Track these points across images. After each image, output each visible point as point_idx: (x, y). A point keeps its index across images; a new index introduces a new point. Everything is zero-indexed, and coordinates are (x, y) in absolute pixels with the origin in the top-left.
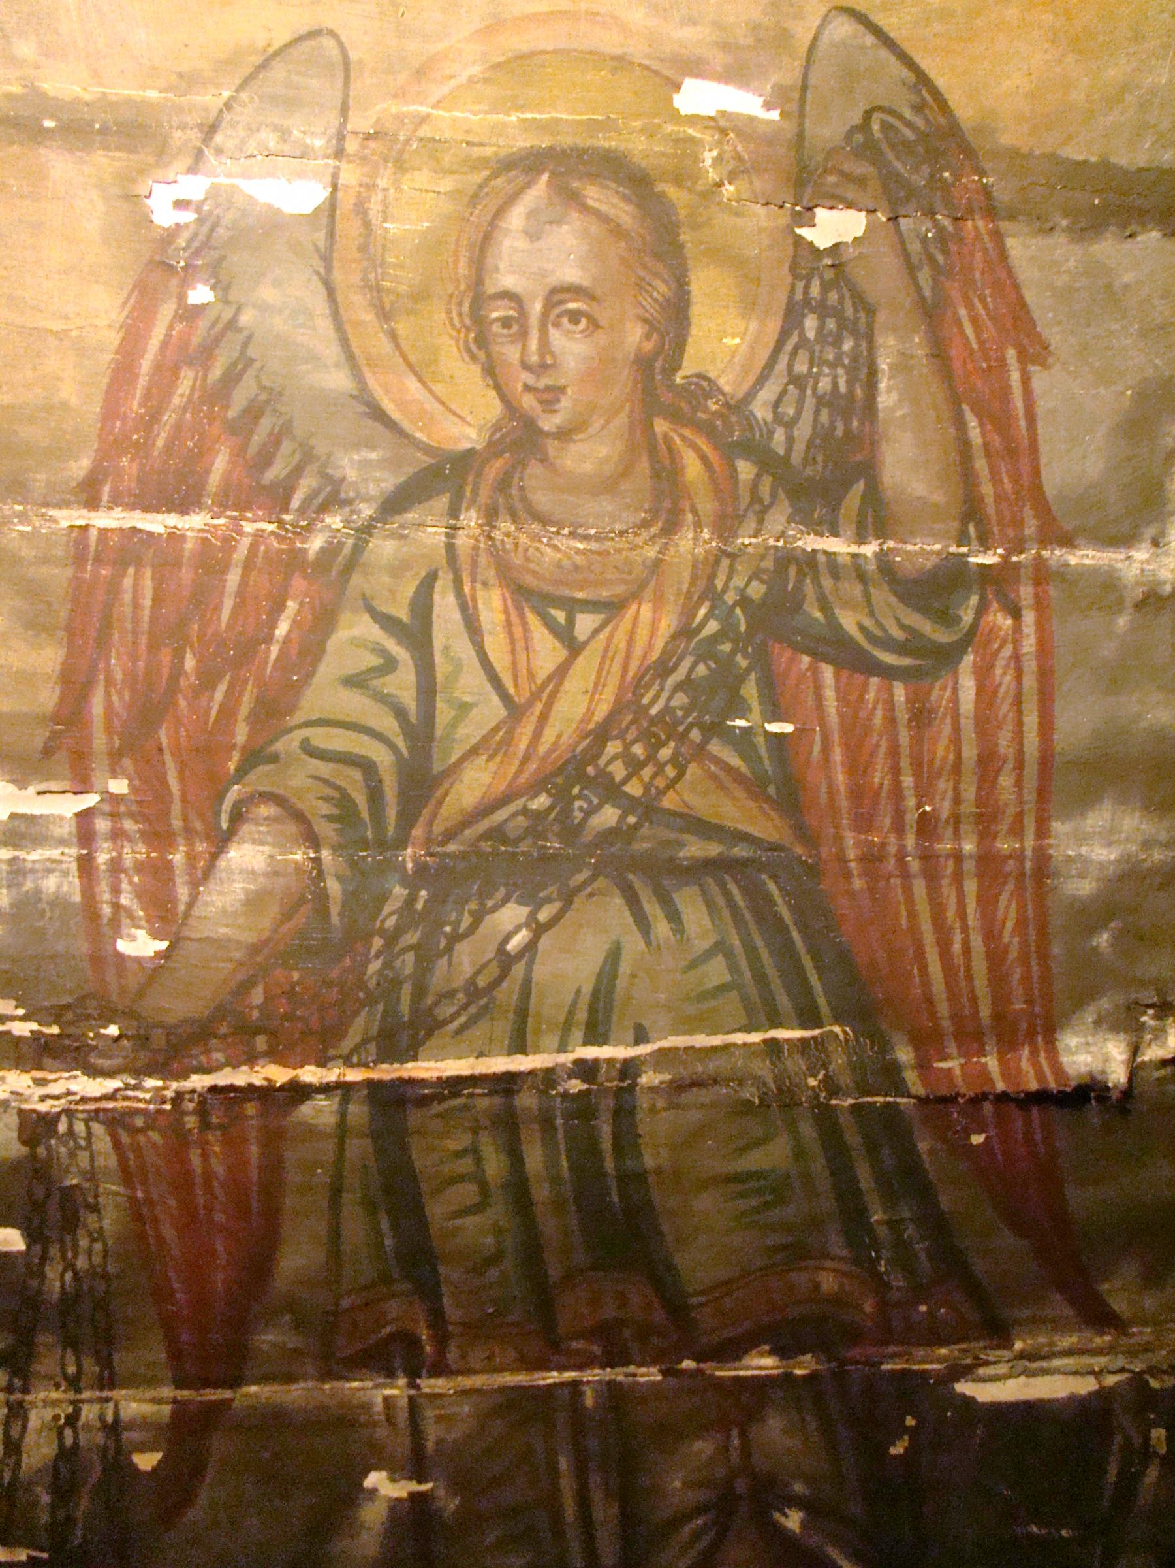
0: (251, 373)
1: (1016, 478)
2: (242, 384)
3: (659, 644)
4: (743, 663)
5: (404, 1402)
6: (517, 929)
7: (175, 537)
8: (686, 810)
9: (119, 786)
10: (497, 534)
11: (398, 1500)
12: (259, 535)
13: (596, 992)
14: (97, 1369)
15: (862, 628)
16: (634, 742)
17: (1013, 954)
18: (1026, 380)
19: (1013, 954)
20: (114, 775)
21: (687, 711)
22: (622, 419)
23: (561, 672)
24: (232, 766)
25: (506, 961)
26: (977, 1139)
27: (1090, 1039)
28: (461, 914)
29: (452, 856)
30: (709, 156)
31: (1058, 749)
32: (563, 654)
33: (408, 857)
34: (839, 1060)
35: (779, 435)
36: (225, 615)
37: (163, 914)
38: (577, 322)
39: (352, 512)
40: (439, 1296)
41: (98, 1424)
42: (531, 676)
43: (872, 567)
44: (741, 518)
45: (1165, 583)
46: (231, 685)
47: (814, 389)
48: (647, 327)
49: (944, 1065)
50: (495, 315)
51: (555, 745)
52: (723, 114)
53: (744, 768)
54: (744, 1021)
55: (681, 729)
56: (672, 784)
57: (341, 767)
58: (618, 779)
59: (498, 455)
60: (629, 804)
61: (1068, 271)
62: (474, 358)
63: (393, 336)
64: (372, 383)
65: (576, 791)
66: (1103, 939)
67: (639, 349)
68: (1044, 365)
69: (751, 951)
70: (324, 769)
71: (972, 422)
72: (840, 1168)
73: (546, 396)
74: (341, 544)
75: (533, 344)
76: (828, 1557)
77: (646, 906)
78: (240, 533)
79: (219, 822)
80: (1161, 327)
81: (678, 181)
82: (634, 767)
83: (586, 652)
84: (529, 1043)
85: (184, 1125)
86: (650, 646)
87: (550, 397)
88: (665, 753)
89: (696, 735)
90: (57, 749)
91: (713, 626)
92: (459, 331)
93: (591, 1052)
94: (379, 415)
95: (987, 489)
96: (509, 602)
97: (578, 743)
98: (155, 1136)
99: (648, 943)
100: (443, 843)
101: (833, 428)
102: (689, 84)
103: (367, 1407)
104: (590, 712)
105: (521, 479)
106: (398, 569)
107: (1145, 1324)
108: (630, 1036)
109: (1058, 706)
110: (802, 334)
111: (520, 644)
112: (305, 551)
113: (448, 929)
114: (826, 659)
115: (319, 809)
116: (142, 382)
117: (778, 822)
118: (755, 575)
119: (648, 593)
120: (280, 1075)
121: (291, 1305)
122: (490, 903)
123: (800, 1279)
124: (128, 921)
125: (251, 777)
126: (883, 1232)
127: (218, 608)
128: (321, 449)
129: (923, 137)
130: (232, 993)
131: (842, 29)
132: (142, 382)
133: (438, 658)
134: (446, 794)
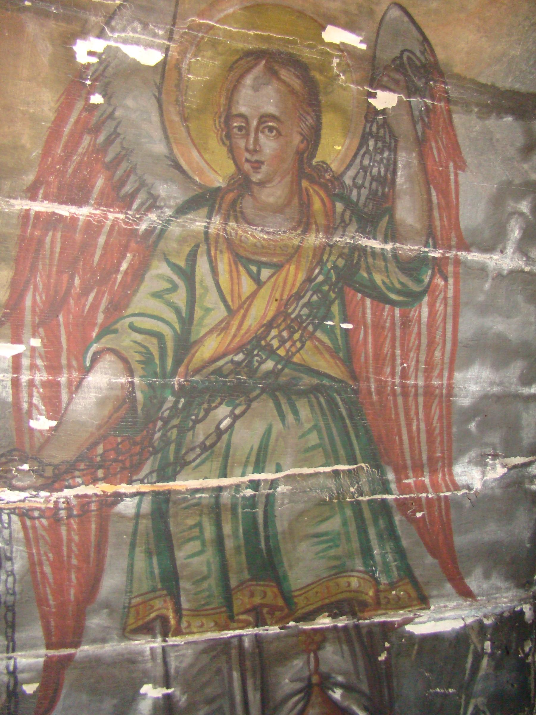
0: (118, 140)
1: (449, 220)
2: (113, 145)
3: (298, 284)
4: (333, 296)
5: (160, 650)
6: (225, 418)
7: (74, 219)
8: (303, 363)
9: (36, 342)
10: (228, 229)
11: (158, 698)
12: (115, 222)
13: (260, 449)
14: (6, 643)
15: (384, 283)
16: (283, 330)
17: (437, 431)
18: (456, 175)
19: (437, 431)
20: (34, 336)
21: (308, 316)
22: (288, 179)
23: (253, 295)
24: (94, 334)
25: (219, 433)
26: (419, 515)
27: (466, 469)
28: (200, 410)
29: (197, 382)
30: (335, 61)
31: (459, 340)
32: (255, 287)
33: (177, 381)
34: (364, 480)
35: (355, 192)
36: (97, 258)
37: (54, 409)
38: (272, 132)
39: (162, 213)
40: (179, 596)
41: (5, 671)
42: (240, 296)
43: (389, 255)
44: (336, 229)
45: (504, 270)
46: (97, 293)
47: (371, 172)
48: (302, 138)
49: (406, 481)
50: (235, 124)
51: (248, 330)
52: (342, 43)
53: (330, 345)
54: (324, 461)
55: (304, 325)
56: (298, 351)
57: (148, 337)
58: (275, 347)
59: (232, 191)
60: (279, 360)
61: (476, 131)
62: (224, 144)
63: (188, 129)
64: (175, 151)
65: (255, 352)
66: (472, 426)
67: (298, 146)
68: (464, 171)
69: (328, 428)
70: (139, 337)
71: (434, 193)
72: (362, 530)
73: (255, 165)
74: (155, 228)
75: (251, 141)
76: (351, 709)
77: (284, 408)
78: (107, 219)
79: (85, 362)
80: (509, 159)
81: (321, 72)
82: (283, 342)
83: (265, 287)
84: (228, 472)
85: (59, 515)
86: (293, 285)
87: (257, 165)
88: (296, 336)
89: (310, 328)
90: (4, 321)
91: (321, 278)
92: (218, 130)
93: (256, 476)
94: (177, 166)
95: (438, 223)
96: (232, 261)
97: (258, 330)
98: (44, 521)
99: (284, 424)
100: (193, 376)
101: (377, 190)
102: (329, 28)
103: (141, 653)
104: (265, 315)
105: (241, 203)
106: (182, 240)
107: (483, 595)
108: (274, 468)
109: (461, 320)
110: (368, 147)
111: (236, 281)
112: (137, 230)
113: (193, 417)
114: (369, 296)
115: (135, 358)
116: (64, 139)
117: (343, 369)
118: (341, 255)
119: (295, 259)
120: (109, 488)
121: (107, 605)
122: (213, 405)
123: (343, 581)
124: (36, 411)
125: (103, 340)
126: (378, 558)
127: (93, 255)
128: (149, 179)
129: (424, 66)
130: (88, 449)
131: (395, 13)
132: (64, 139)
133: (197, 285)
134: (196, 352)
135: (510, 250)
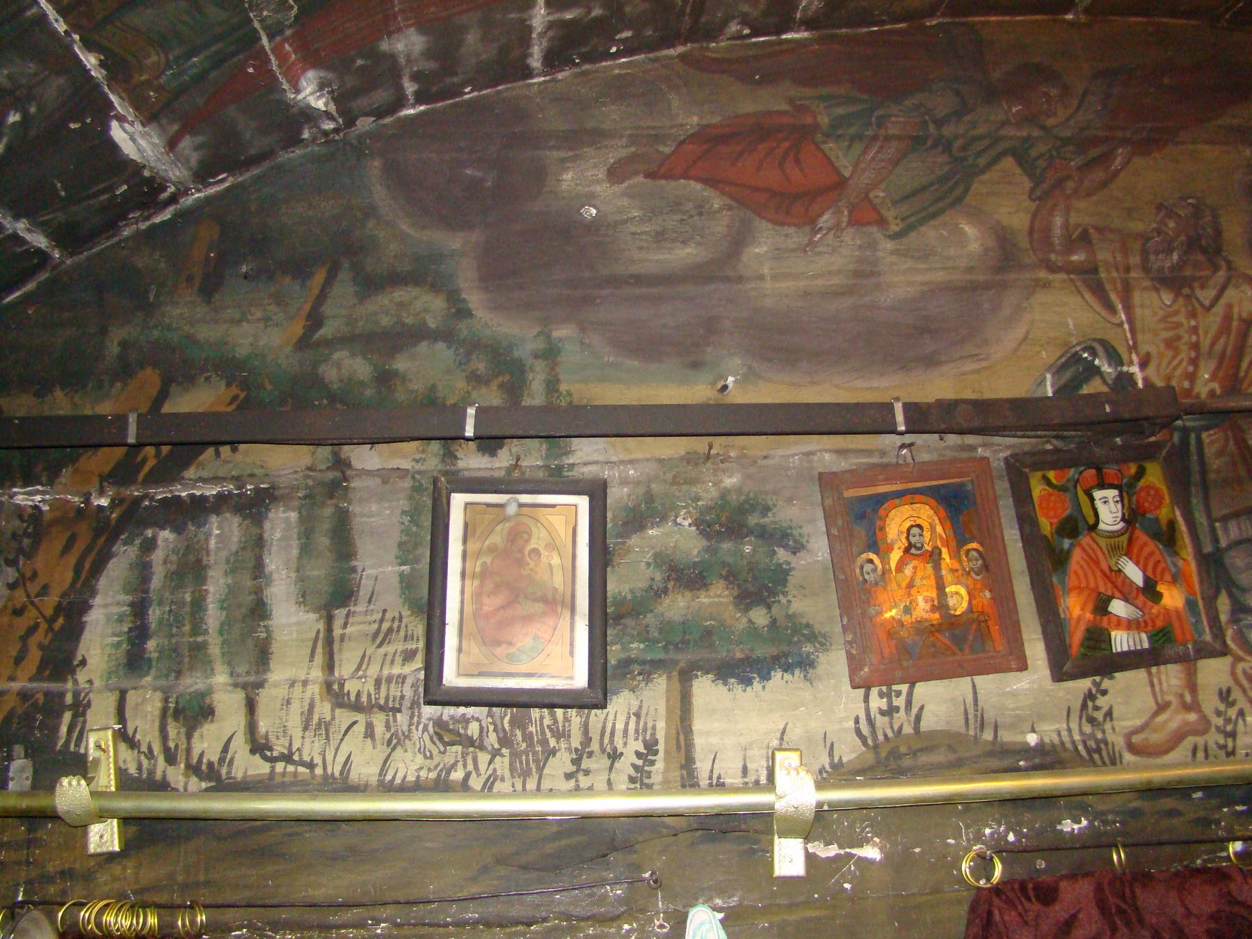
135: (551, 18)
